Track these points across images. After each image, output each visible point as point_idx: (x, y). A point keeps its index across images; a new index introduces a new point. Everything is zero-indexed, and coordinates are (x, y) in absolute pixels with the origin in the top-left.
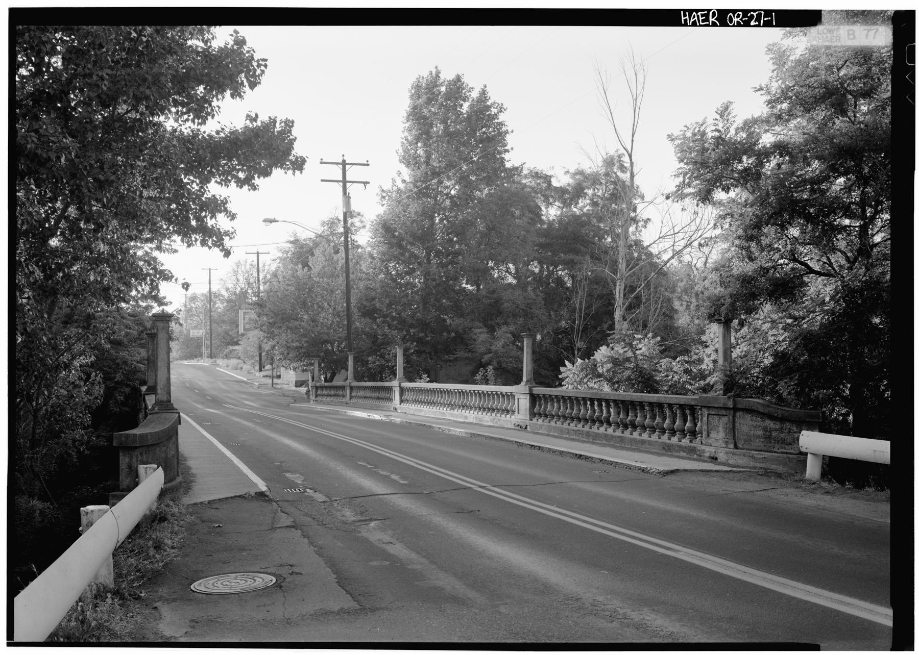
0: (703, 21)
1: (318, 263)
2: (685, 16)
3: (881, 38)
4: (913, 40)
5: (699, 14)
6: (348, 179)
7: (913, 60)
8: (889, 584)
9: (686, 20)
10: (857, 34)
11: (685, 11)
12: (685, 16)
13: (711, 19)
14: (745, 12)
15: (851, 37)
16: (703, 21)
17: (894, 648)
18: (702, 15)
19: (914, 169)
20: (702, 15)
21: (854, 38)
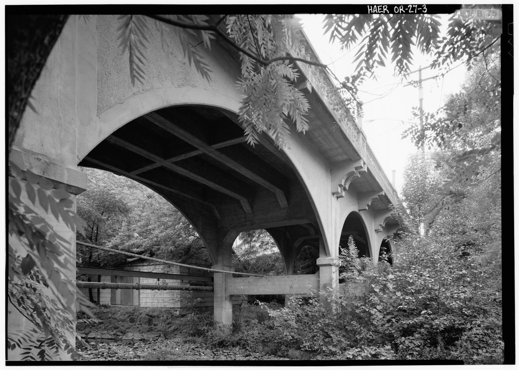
0: (380, 10)
1: (261, 262)
2: (370, 8)
3: (498, 15)
4: (512, 21)
5: (378, 7)
6: (142, 291)
7: (512, 32)
8: (101, 16)
9: (370, 11)
10: (483, 13)
11: (370, 5)
12: (370, 8)
13: (384, 10)
14: (405, 6)
15: (480, 15)
16: (380, 10)
17: (505, 363)
18: (380, 8)
19: (513, 94)
20: (380, 8)
21: (481, 16)
